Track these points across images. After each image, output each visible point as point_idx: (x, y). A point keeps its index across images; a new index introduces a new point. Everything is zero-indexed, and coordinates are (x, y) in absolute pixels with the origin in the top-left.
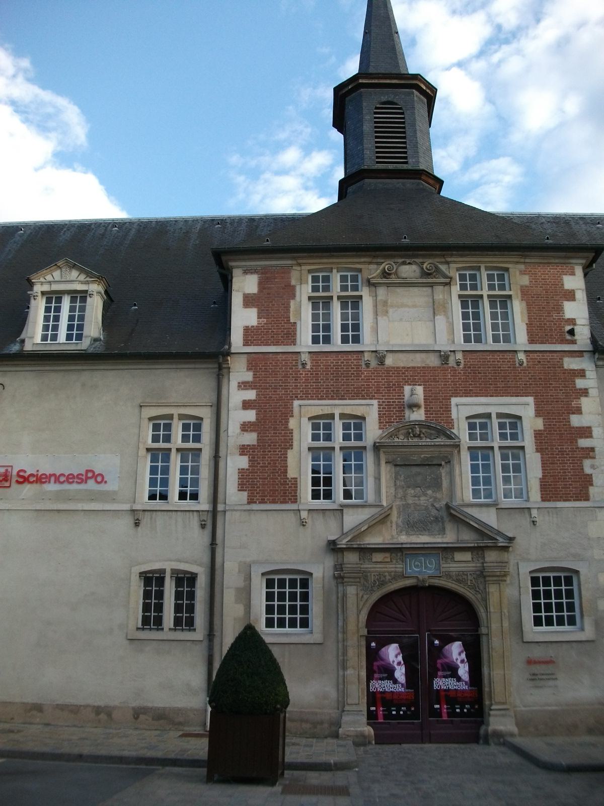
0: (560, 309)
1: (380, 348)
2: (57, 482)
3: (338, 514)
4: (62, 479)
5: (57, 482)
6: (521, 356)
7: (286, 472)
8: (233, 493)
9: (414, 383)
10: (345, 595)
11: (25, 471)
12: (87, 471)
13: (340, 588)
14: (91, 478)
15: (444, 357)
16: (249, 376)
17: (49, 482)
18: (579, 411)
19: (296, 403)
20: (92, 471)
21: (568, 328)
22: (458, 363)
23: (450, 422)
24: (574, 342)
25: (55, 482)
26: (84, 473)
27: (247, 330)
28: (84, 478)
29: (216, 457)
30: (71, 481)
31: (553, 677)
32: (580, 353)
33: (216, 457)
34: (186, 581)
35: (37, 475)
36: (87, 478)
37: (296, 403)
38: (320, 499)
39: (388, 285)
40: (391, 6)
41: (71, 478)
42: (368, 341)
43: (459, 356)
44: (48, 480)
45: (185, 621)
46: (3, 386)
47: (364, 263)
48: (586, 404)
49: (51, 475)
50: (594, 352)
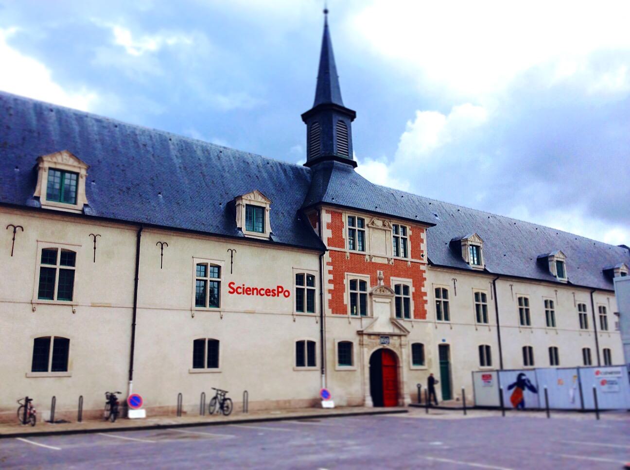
0: (332, 297)
1: (372, 254)
2: (259, 294)
3: (360, 320)
4: (263, 292)
5: (259, 294)
6: (409, 263)
7: (343, 302)
8: (327, 311)
9: (380, 269)
10: (363, 352)
11: (233, 284)
12: (278, 287)
13: (362, 349)
14: (281, 292)
15: (389, 260)
16: (330, 260)
17: (253, 294)
18: (423, 286)
19: (346, 273)
20: (282, 288)
21: (421, 254)
22: (392, 263)
23: (390, 286)
24: (422, 259)
25: (257, 294)
26: (276, 289)
27: (329, 239)
28: (276, 292)
29: (321, 294)
30: (268, 294)
31: (528, 350)
32: (424, 264)
33: (321, 294)
34: (312, 344)
35: (244, 288)
36: (279, 292)
37: (346, 273)
38: (52, 299)
39: (373, 228)
40: (352, 144)
41: (268, 292)
42: (367, 252)
43: (393, 260)
44: (251, 292)
45: (311, 309)
46: (8, 226)
47: (365, 217)
48: (425, 283)
49: (253, 289)
50: (428, 264)
